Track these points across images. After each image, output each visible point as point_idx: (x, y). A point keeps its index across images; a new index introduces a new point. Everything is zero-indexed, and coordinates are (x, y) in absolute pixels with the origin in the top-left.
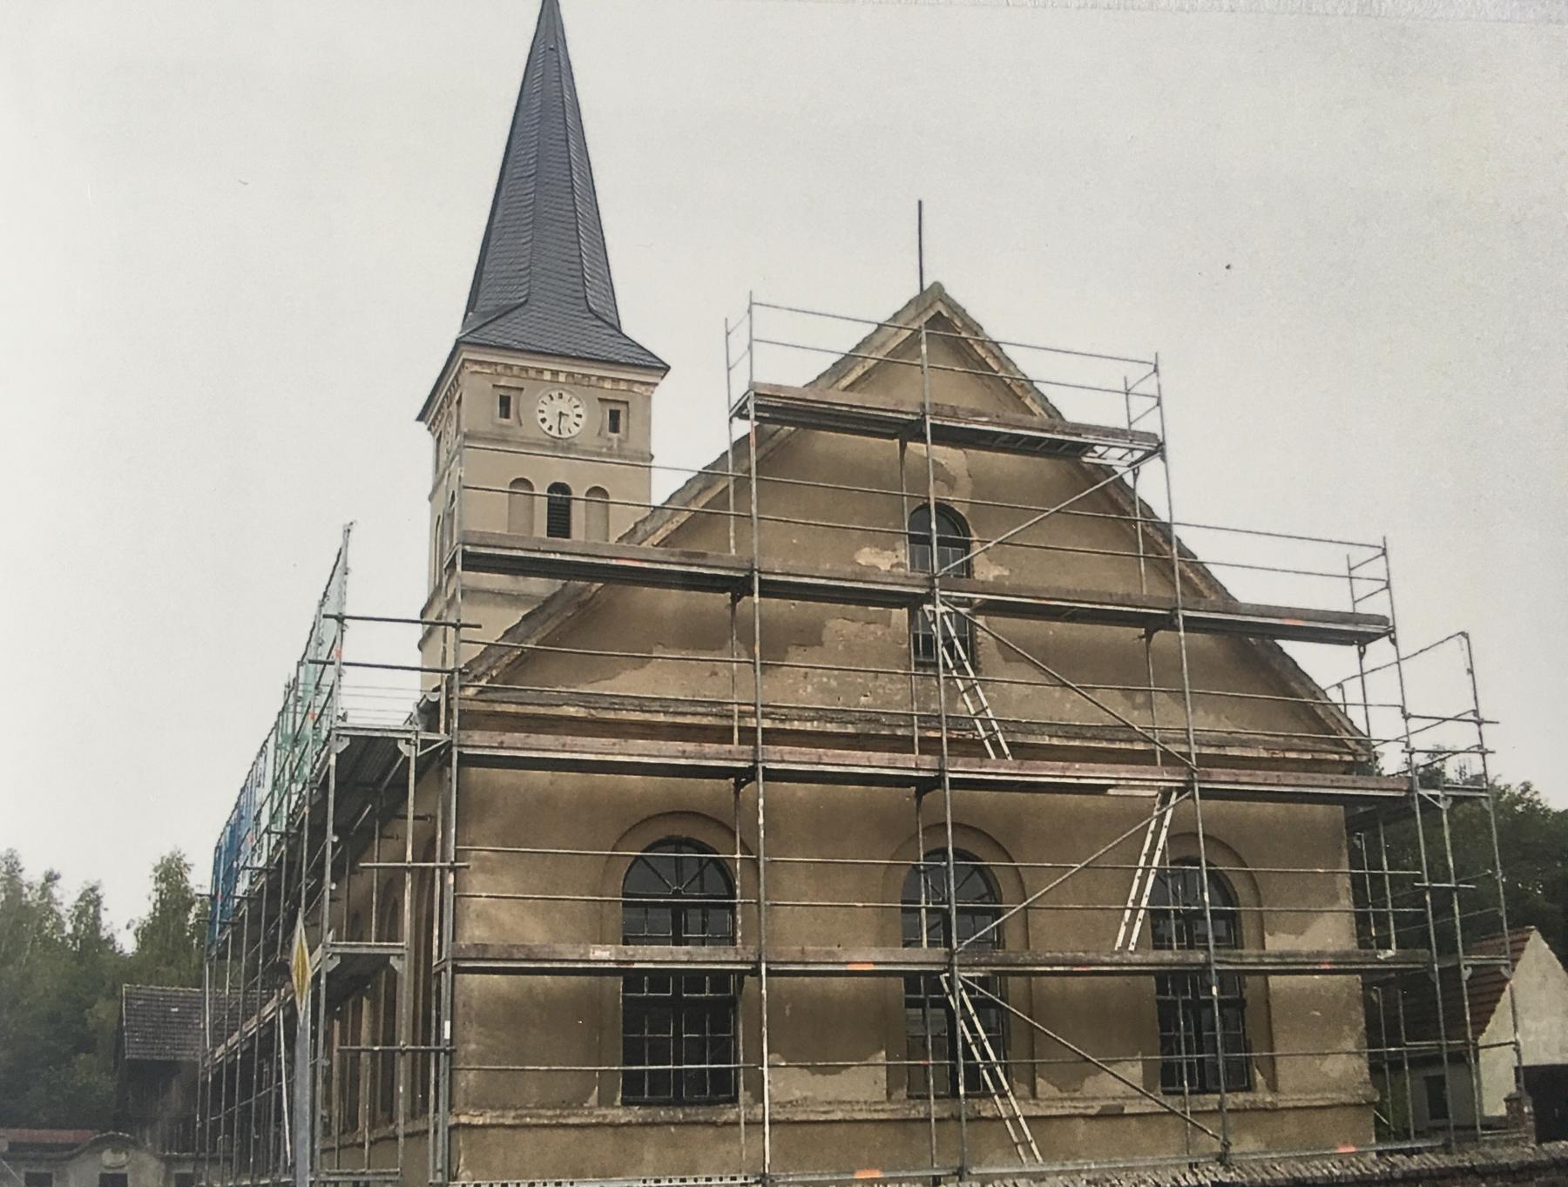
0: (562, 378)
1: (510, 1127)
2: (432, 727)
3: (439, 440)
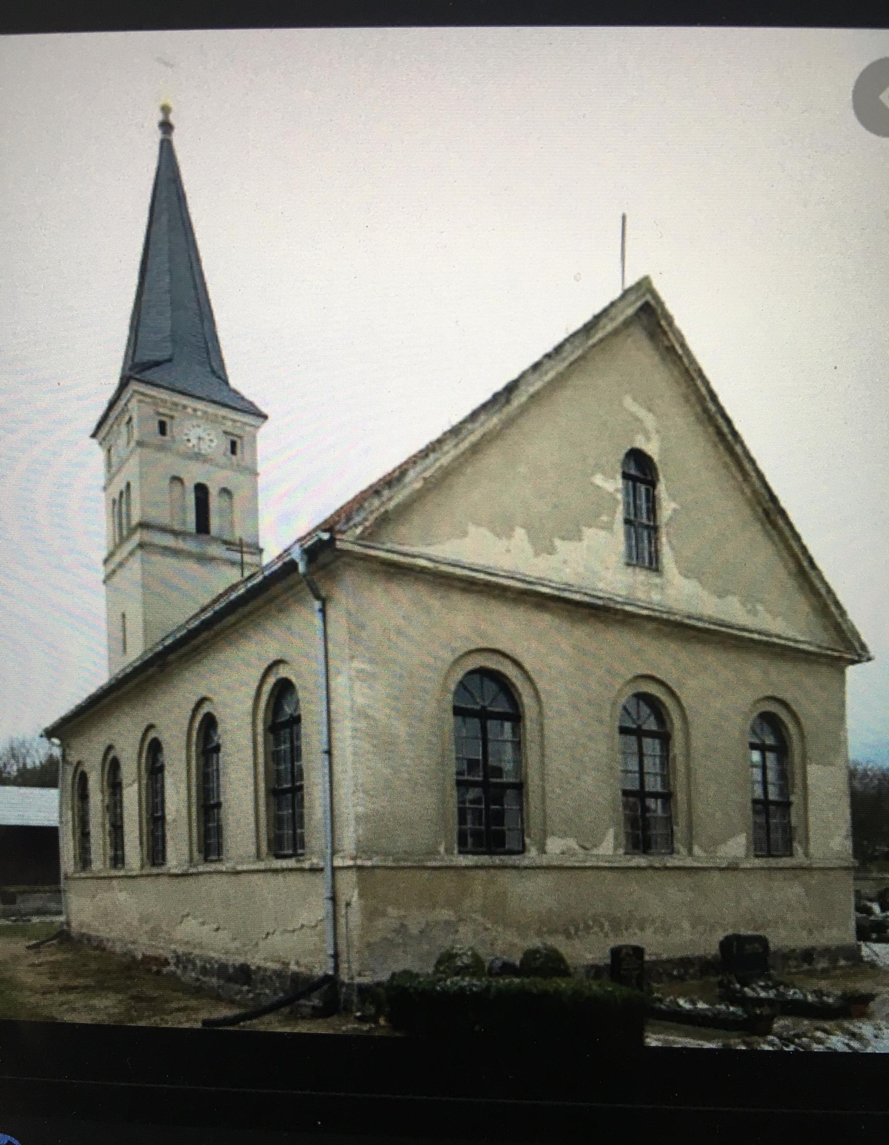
0: (199, 413)
1: (392, 868)
2: (673, 1033)
3: (109, 451)
